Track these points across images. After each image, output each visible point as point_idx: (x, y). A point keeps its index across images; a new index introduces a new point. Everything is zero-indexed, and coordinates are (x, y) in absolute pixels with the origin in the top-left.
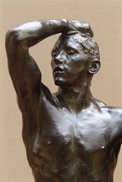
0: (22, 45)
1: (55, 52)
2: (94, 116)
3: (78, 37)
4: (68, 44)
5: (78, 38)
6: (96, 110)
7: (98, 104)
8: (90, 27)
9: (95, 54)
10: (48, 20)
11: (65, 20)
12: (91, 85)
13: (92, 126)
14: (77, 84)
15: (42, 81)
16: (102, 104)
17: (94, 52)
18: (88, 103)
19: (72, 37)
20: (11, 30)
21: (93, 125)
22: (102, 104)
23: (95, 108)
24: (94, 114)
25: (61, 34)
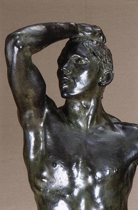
0: (25, 51)
1: (62, 60)
2: (106, 133)
3: (88, 43)
4: (77, 51)
5: (88, 44)
6: (109, 127)
7: (111, 120)
8: (101, 31)
9: (108, 62)
10: (54, 23)
11: (73, 24)
12: (102, 98)
13: (103, 144)
14: (86, 97)
15: (47, 93)
16: (115, 120)
17: (106, 60)
18: (99, 118)
19: (82, 43)
20: (12, 35)
21: (105, 144)
22: (115, 120)
23: (107, 124)
24: (105, 131)
25: (68, 39)
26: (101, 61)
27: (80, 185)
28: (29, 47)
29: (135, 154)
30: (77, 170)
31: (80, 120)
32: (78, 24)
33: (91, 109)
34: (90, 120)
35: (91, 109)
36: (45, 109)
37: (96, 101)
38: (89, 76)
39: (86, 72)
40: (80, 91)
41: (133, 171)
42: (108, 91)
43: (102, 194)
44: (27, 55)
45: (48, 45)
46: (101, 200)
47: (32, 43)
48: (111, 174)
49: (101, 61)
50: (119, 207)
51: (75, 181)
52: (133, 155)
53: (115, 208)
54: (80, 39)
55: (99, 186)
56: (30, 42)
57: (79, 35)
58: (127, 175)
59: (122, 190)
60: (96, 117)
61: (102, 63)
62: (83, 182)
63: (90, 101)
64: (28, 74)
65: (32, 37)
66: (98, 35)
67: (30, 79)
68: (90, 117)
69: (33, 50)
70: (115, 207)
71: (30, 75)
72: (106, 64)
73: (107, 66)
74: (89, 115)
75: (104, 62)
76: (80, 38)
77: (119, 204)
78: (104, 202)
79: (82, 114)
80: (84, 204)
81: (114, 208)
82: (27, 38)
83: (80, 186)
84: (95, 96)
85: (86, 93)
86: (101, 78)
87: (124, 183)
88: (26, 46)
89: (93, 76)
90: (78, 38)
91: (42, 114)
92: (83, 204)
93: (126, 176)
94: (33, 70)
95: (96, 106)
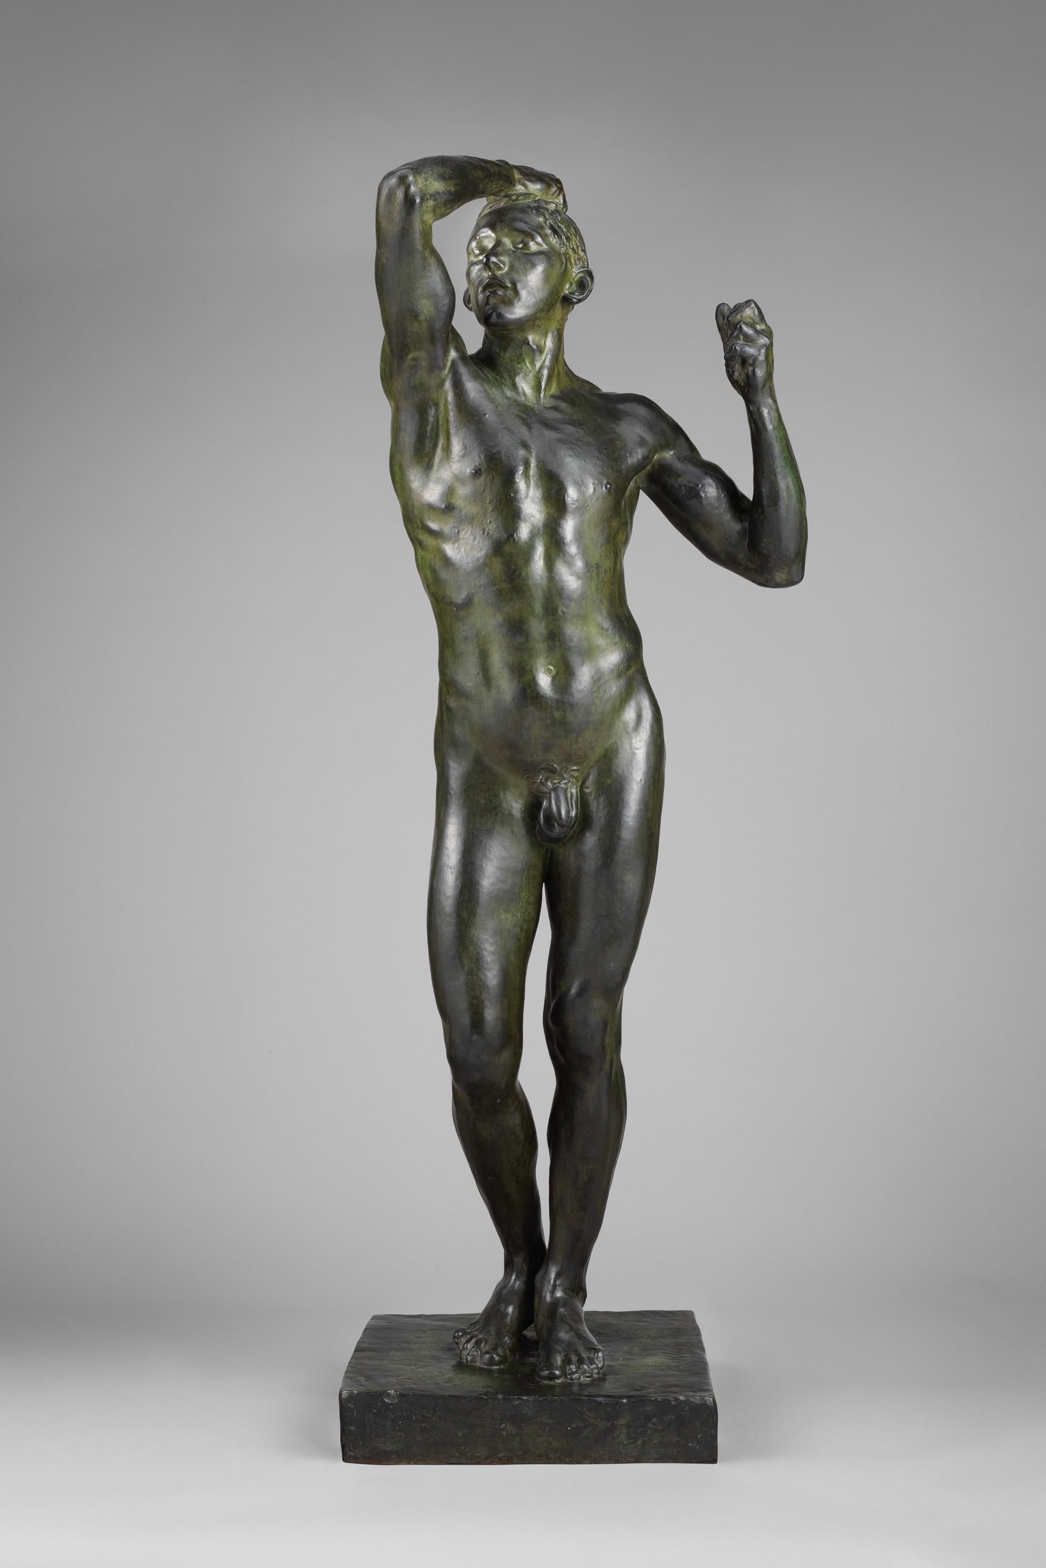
0: (424, 211)
9: (580, 252)
26: (568, 248)
27: (533, 516)
28: (431, 203)
29: (642, 456)
30: (526, 483)
31: (524, 378)
32: (516, 167)
33: (547, 354)
34: (545, 378)
35: (547, 354)
36: (449, 351)
37: (557, 339)
38: (547, 277)
39: (540, 269)
40: (528, 311)
41: (634, 499)
42: (577, 318)
43: (579, 536)
44: (427, 220)
45: (462, 205)
46: (578, 548)
47: (438, 193)
48: (597, 493)
49: (568, 248)
50: (613, 569)
51: (522, 506)
52: (640, 457)
53: (606, 571)
54: (520, 198)
55: (573, 519)
56: (434, 192)
57: (516, 190)
58: (625, 502)
59: (617, 533)
60: (556, 373)
61: (571, 252)
62: (539, 509)
63: (545, 335)
64: (426, 265)
65: (438, 180)
66: (555, 192)
67: (429, 277)
68: (545, 372)
69: (438, 211)
70: (605, 567)
71: (430, 268)
72: (576, 256)
73: (579, 260)
74: (541, 368)
75: (573, 249)
76: (519, 196)
77: (612, 562)
78: (584, 552)
79: (527, 364)
80: (542, 557)
81: (603, 570)
82: (428, 182)
83: (532, 519)
84: (554, 326)
85: (538, 315)
86: (568, 286)
87: (620, 518)
88: (428, 199)
89: (554, 279)
90: (513, 195)
91: (445, 361)
92: (540, 555)
93: (623, 503)
94: (435, 257)
95: (557, 348)
